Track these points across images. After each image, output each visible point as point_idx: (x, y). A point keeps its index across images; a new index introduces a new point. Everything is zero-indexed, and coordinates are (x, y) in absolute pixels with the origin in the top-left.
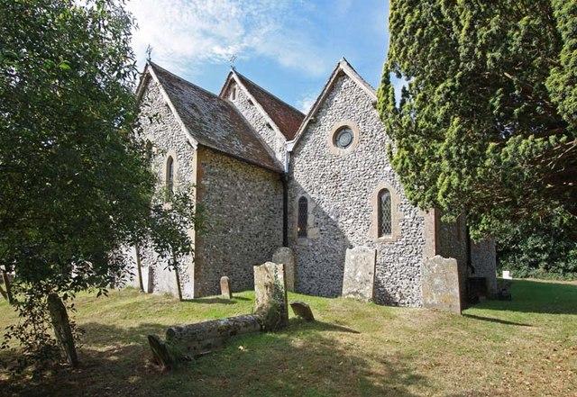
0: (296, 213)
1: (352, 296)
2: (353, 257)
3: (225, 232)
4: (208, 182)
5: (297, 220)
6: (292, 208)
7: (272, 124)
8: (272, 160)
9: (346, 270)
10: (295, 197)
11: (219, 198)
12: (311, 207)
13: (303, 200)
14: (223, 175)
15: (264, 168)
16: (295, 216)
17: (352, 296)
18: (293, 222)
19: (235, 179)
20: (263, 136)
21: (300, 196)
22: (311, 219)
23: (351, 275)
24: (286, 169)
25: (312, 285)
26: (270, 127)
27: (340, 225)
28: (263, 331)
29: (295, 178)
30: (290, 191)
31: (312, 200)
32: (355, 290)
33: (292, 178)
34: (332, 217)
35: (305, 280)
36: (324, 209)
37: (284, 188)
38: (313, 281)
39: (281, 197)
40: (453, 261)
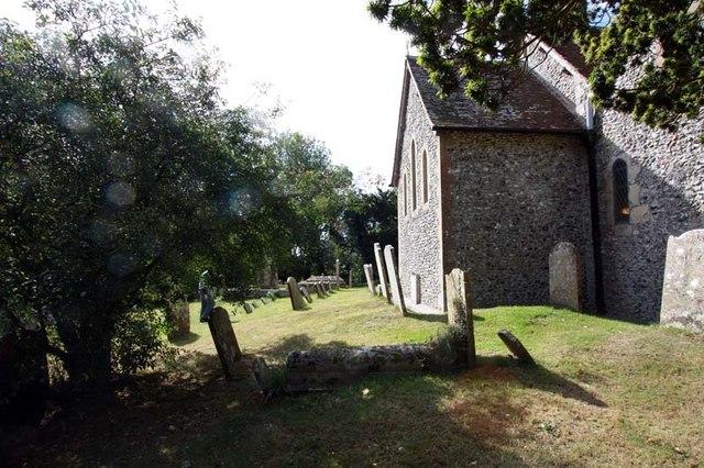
0: (610, 186)
1: (679, 325)
2: (681, 251)
3: (487, 228)
4: (458, 171)
5: (612, 196)
6: (603, 181)
7: (570, 68)
8: (571, 117)
9: (668, 276)
10: (606, 164)
11: (475, 187)
12: (632, 172)
13: (621, 166)
14: (479, 158)
15: (552, 133)
16: (608, 195)
17: (679, 325)
18: (606, 203)
19: (502, 158)
20: (562, 89)
21: (614, 159)
22: (634, 192)
23: (678, 284)
24: (588, 125)
25: (644, 299)
26: (569, 74)
27: (688, 193)
28: (426, 371)
29: (605, 133)
30: (600, 156)
31: (635, 161)
32: (686, 314)
33: (601, 136)
34: (672, 183)
35: (630, 291)
36: (656, 172)
37: (589, 153)
38: (644, 293)
39: (585, 167)
40: (671, 240)
